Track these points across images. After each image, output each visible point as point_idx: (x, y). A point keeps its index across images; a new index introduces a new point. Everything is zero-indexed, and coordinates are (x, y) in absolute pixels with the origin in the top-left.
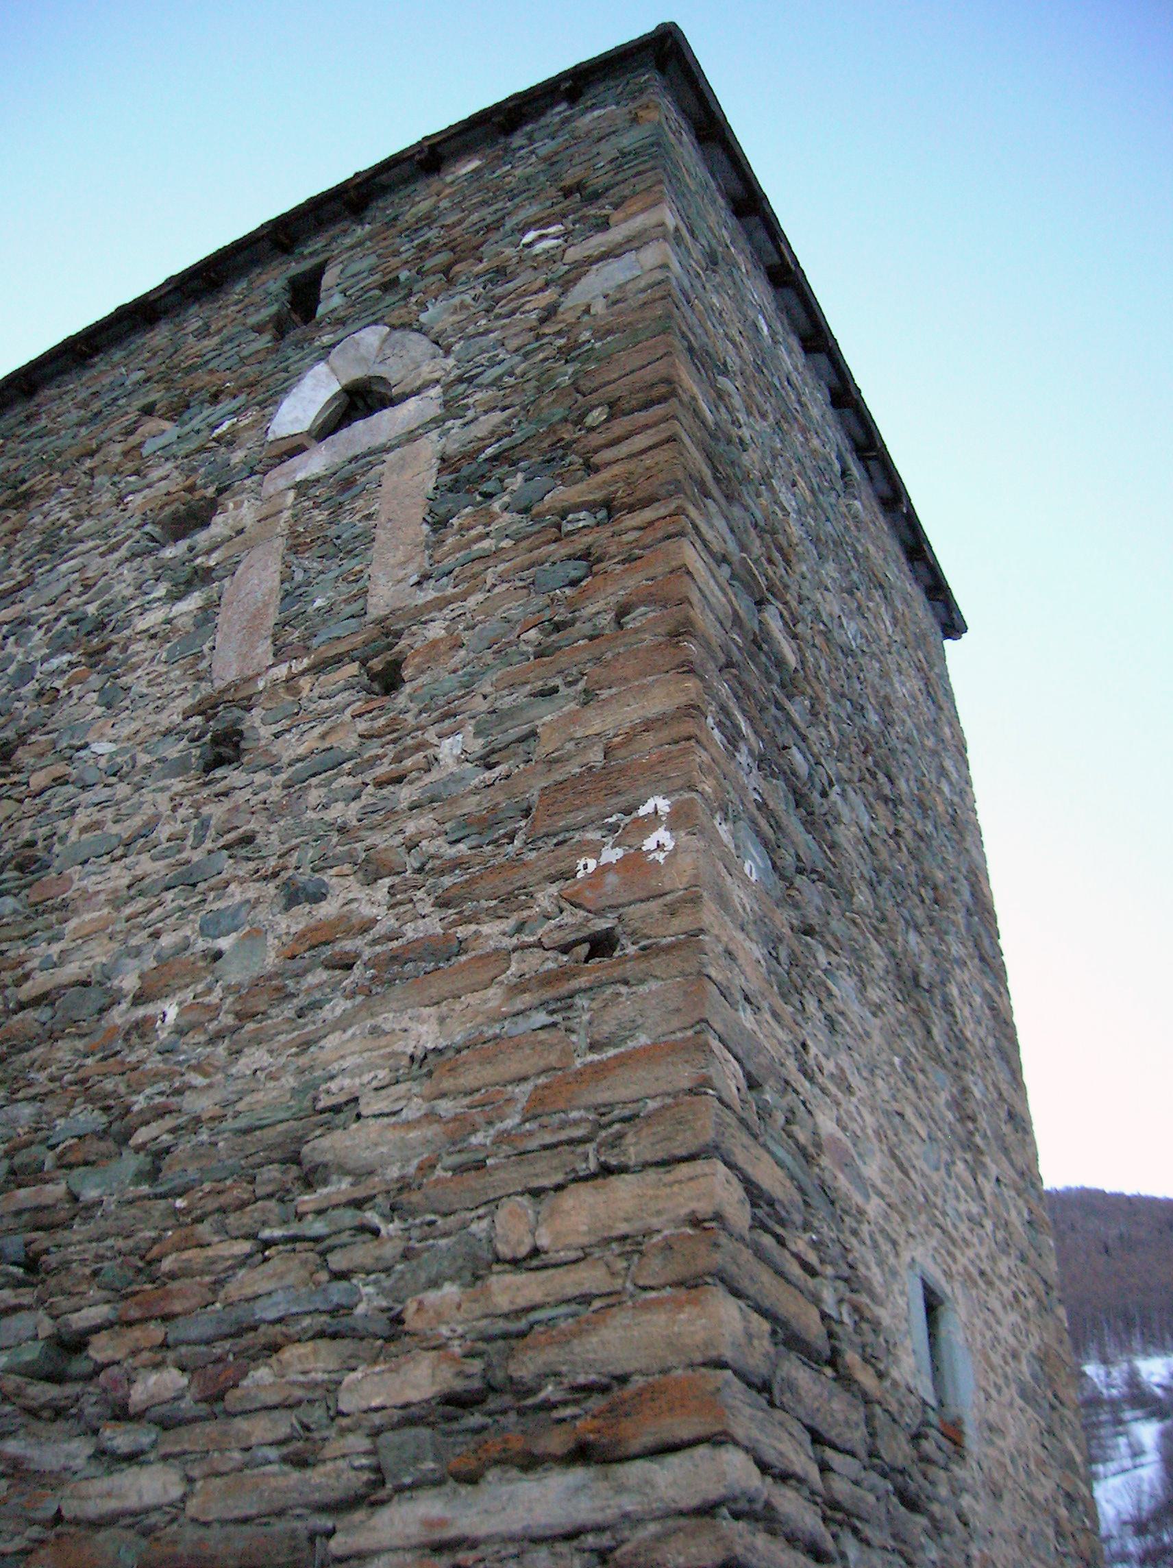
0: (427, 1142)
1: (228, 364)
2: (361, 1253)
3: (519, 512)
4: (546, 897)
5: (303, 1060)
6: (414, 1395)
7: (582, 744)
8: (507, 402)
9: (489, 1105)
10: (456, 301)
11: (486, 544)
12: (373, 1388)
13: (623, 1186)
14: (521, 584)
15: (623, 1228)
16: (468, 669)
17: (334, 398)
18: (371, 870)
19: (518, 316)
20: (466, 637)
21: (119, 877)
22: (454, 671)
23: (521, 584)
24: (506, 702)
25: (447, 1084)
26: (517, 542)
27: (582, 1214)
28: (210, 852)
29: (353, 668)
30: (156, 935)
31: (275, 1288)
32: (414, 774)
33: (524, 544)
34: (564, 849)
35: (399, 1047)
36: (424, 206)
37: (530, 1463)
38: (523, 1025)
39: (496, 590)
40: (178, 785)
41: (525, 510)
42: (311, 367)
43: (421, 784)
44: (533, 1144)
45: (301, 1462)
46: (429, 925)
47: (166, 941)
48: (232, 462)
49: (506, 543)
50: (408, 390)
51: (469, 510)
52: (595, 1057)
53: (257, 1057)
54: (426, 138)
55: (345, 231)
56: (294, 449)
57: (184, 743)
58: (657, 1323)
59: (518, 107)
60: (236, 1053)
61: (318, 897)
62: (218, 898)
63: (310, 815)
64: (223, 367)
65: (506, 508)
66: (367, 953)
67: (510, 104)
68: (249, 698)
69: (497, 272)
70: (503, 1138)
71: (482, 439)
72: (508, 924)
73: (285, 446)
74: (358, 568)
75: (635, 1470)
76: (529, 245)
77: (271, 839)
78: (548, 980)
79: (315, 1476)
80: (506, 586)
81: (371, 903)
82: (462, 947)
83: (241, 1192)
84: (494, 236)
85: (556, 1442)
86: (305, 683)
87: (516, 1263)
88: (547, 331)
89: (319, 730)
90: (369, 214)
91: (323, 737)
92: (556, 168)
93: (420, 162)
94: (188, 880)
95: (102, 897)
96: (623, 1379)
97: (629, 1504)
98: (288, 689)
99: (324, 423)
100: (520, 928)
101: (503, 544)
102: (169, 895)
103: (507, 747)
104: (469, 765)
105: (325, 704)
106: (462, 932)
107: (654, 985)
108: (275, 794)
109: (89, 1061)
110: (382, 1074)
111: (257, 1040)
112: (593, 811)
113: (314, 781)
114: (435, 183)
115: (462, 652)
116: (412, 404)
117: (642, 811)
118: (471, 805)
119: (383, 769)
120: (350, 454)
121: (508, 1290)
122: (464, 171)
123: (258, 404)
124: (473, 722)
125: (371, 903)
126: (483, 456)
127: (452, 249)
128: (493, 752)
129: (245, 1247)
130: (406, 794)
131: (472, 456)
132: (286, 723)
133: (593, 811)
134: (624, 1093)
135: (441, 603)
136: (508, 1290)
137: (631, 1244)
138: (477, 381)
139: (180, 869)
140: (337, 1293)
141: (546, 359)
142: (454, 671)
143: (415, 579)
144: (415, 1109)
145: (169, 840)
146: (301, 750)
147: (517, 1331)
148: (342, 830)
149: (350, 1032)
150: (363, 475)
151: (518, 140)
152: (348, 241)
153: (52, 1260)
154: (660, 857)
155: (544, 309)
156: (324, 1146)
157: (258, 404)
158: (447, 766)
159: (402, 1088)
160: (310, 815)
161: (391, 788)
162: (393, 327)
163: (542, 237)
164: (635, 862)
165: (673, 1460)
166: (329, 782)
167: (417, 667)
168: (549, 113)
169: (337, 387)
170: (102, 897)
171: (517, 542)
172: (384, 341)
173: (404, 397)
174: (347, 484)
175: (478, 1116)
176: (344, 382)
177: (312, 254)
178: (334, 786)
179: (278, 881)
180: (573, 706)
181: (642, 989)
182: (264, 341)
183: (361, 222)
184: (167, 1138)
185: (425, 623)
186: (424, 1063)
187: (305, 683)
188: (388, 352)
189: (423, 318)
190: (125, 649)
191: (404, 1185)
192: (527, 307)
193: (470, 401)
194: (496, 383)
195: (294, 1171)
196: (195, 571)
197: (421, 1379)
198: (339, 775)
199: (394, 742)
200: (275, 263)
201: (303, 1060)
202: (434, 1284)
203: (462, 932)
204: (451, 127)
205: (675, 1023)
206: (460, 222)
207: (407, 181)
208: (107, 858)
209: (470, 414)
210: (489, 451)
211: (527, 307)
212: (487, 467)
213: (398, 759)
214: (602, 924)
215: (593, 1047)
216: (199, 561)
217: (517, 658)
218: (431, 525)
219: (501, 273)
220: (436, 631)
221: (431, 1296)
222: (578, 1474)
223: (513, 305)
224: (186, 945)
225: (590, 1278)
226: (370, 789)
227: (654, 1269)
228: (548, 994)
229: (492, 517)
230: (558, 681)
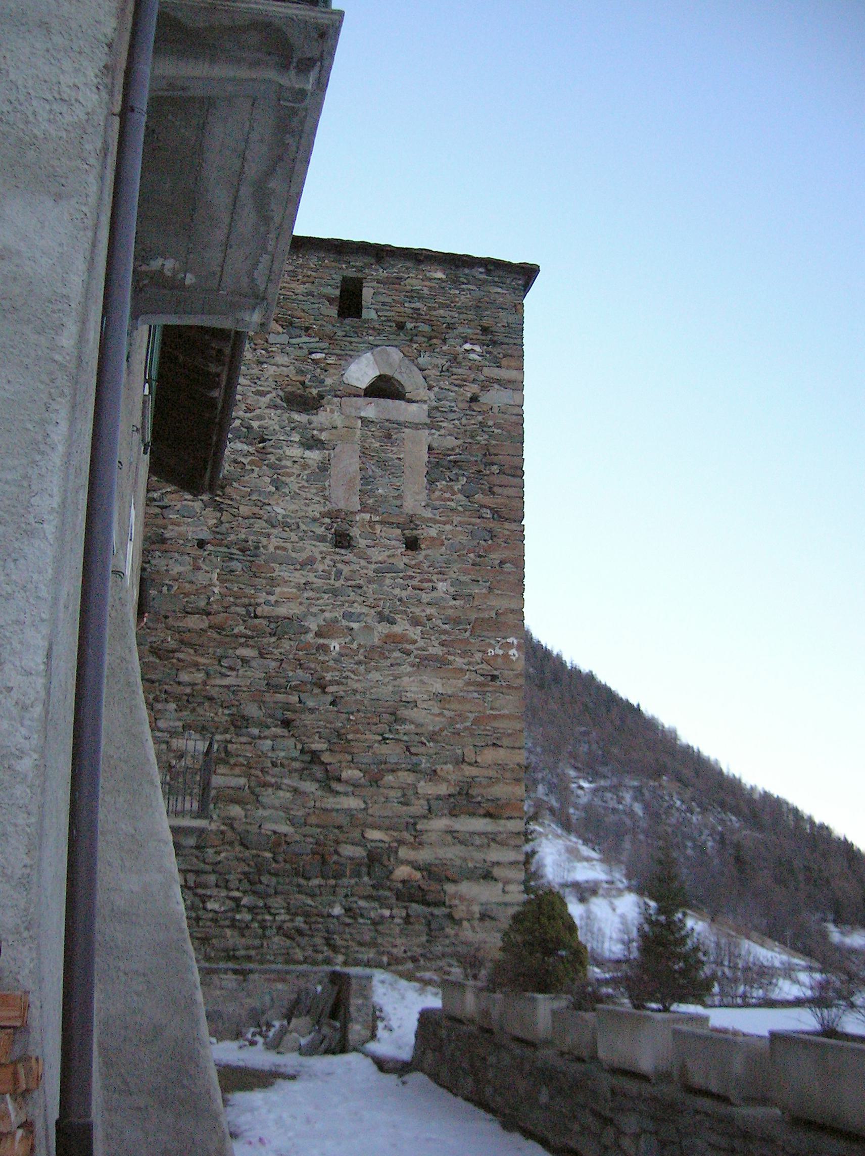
0: (441, 722)
2: (421, 750)
4: (478, 656)
5: (396, 683)
6: (442, 793)
7: (491, 608)
9: (461, 716)
12: (427, 788)
13: (501, 751)
15: (500, 762)
18: (415, 622)
21: (299, 577)
25: (447, 706)
27: (489, 756)
29: (399, 531)
30: (323, 611)
31: (392, 752)
34: (483, 643)
35: (430, 689)
37: (472, 814)
38: (470, 696)
44: (476, 733)
45: (406, 804)
46: (436, 650)
47: (327, 615)
49: (460, 508)
52: (492, 712)
53: (375, 676)
58: (509, 789)
60: (368, 671)
61: (393, 622)
62: (349, 607)
66: (415, 652)
67: (309, 121)
70: (466, 728)
72: (466, 661)
75: (502, 822)
77: (370, 589)
78: (480, 684)
79: (411, 809)
81: (415, 633)
82: (450, 663)
83: (376, 720)
85: (482, 811)
86: (378, 527)
87: (470, 764)
91: (389, 557)
94: (335, 593)
95: (293, 584)
96: (498, 799)
97: (501, 829)
100: (469, 664)
102: (326, 596)
106: (451, 658)
107: (511, 697)
109: (301, 653)
110: (425, 696)
111: (377, 669)
112: (493, 634)
117: (508, 640)
118: (450, 612)
119: (415, 582)
121: (469, 771)
125: (415, 633)
129: (380, 738)
130: (425, 597)
133: (493, 634)
134: (501, 725)
136: (469, 771)
137: (502, 767)
140: (415, 759)
144: (436, 710)
147: (471, 782)
148: (400, 600)
149: (412, 679)
153: (297, 723)
154: (514, 658)
156: (405, 713)
159: (430, 703)
164: (506, 656)
165: (512, 821)
169: (378, 374)
170: (293, 584)
175: (458, 719)
179: (375, 610)
180: (484, 591)
181: (507, 697)
184: (342, 694)
186: (441, 698)
187: (378, 527)
190: (280, 460)
191: (434, 733)
192: (467, 389)
195: (393, 718)
197: (443, 789)
201: (396, 683)
202: (446, 763)
203: (451, 658)
205: (517, 710)
208: (292, 567)
211: (467, 389)
214: (495, 673)
215: (492, 709)
220: (433, 532)
221: (444, 767)
222: (488, 820)
224: (335, 620)
225: (492, 773)
227: (508, 775)
228: (479, 689)
230: (479, 579)
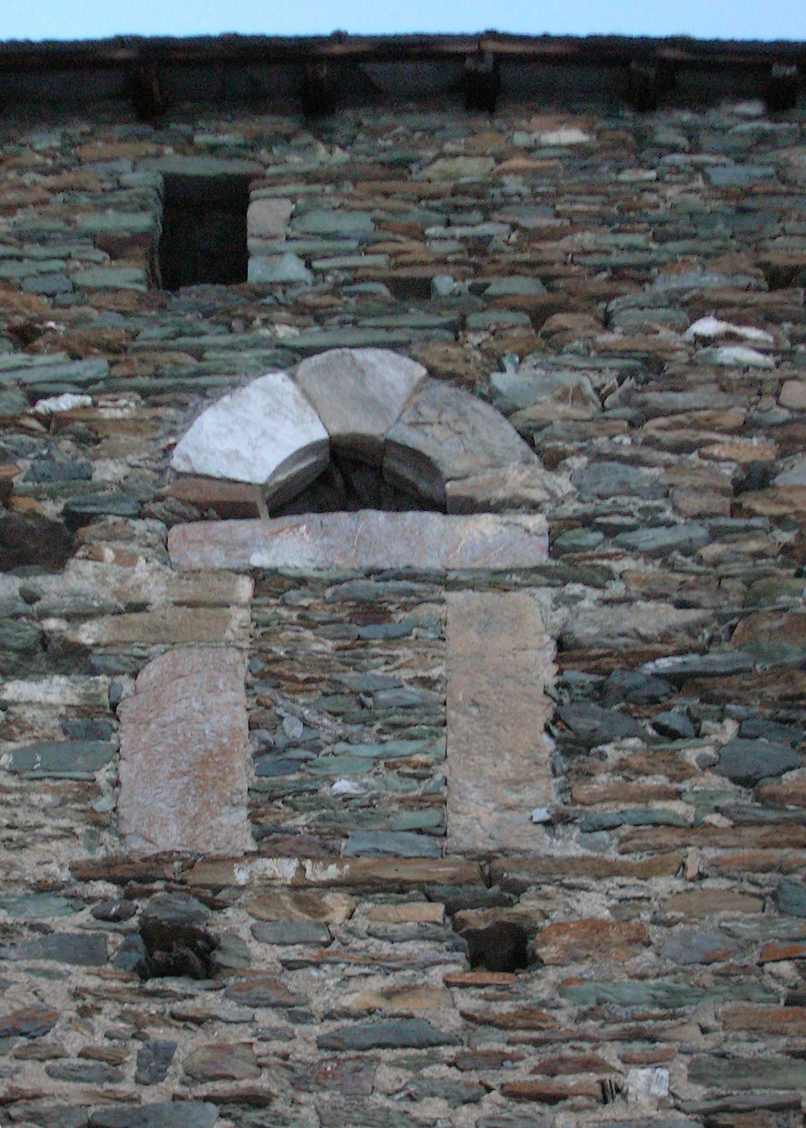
1: (49, 285)
3: (735, 780)
8: (692, 596)
10: (568, 379)
11: (678, 807)
14: (753, 889)
16: (667, 981)
17: (312, 448)
19: (694, 456)
20: (656, 933)
22: (642, 977)
23: (753, 889)
24: (746, 1050)
26: (738, 824)
28: (176, 1097)
29: (437, 911)
32: (580, 1100)
33: (750, 833)
36: (472, 169)
39: (708, 884)
40: (82, 977)
41: (747, 782)
42: (259, 372)
43: (596, 1116)
48: (97, 477)
49: (722, 822)
50: (481, 498)
51: (633, 742)
54: (492, 35)
55: (430, 132)
56: (228, 504)
57: (85, 916)
59: (678, 65)
63: (379, 1099)
64: (32, 284)
65: (709, 765)
67: (669, 53)
68: (217, 890)
69: (646, 361)
71: (645, 639)
73: (217, 494)
74: (421, 758)
76: (705, 341)
80: (725, 884)
84: (632, 295)
88: (758, 507)
89: (389, 982)
90: (345, 120)
91: (389, 994)
92: (750, 223)
93: (469, 75)
98: (298, 902)
99: (286, 484)
101: (714, 819)
103: (751, 1110)
104: (682, 1116)
105: (386, 948)
108: (304, 1052)
113: (386, 1054)
114: (488, 133)
115: (649, 955)
116: (485, 526)
119: (520, 1075)
120: (367, 562)
122: (552, 138)
123: (144, 393)
124: (687, 1059)
126: (650, 667)
127: (547, 280)
128: (726, 1109)
131: (634, 660)
132: (310, 953)
135: (604, 870)
138: (622, 537)
139: (113, 1106)
141: (759, 555)
142: (642, 977)
143: (541, 814)
145: (80, 1055)
146: (349, 1001)
150: (405, 607)
151: (666, 127)
152: (295, 161)
155: (746, 467)
157: (144, 393)
158: (637, 1105)
160: (379, 1099)
161: (536, 1106)
162: (432, 372)
163: (731, 338)
166: (416, 1066)
167: (566, 948)
168: (726, 108)
169: (319, 434)
171: (738, 824)
172: (417, 390)
173: (469, 507)
174: (372, 611)
176: (336, 428)
177: (213, 150)
178: (426, 1072)
182: (129, 275)
183: (325, 135)
185: (571, 887)
188: (428, 413)
189: (498, 380)
193: (617, 566)
194: (661, 554)
196: (44, 639)
198: (433, 1059)
199: (537, 1043)
200: (119, 130)
204: (546, 38)
206: (554, 235)
207: (423, 99)
209: (616, 589)
210: (664, 664)
212: (662, 688)
213: (549, 1069)
216: (52, 624)
217: (758, 994)
218: (558, 741)
219: (652, 366)
220: (594, 904)
223: (686, 435)
226: (495, 1095)
229: (682, 772)
